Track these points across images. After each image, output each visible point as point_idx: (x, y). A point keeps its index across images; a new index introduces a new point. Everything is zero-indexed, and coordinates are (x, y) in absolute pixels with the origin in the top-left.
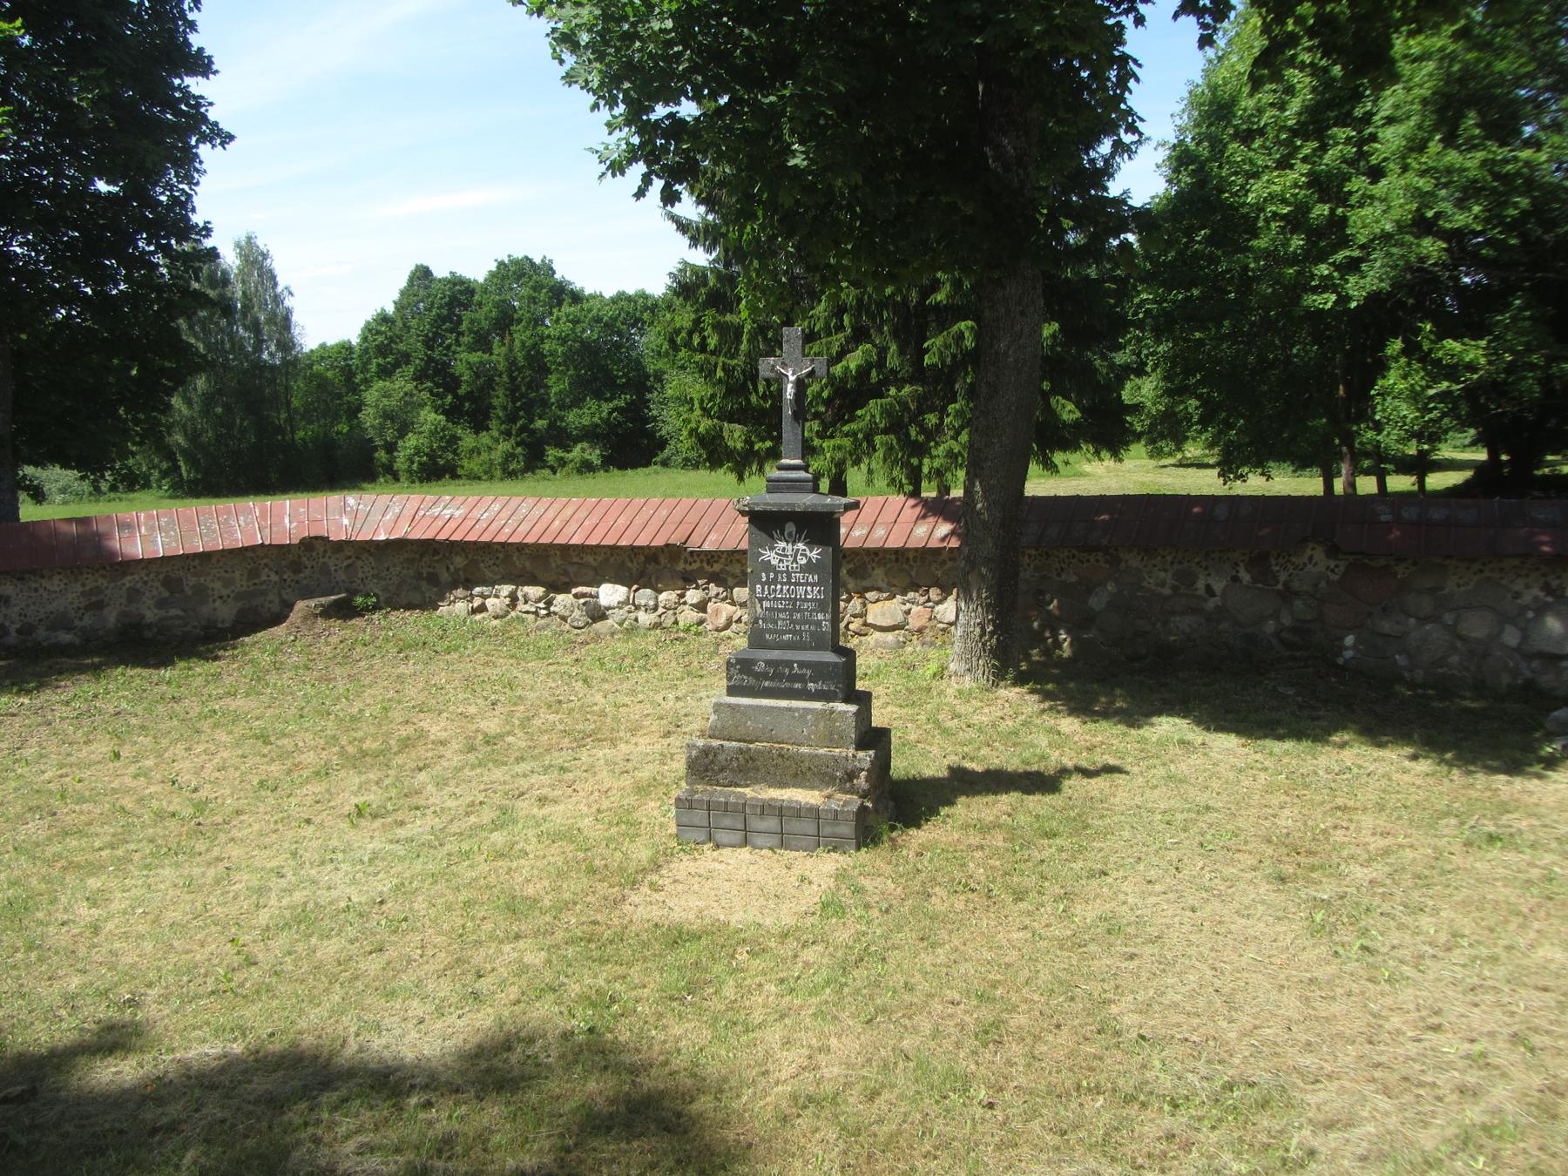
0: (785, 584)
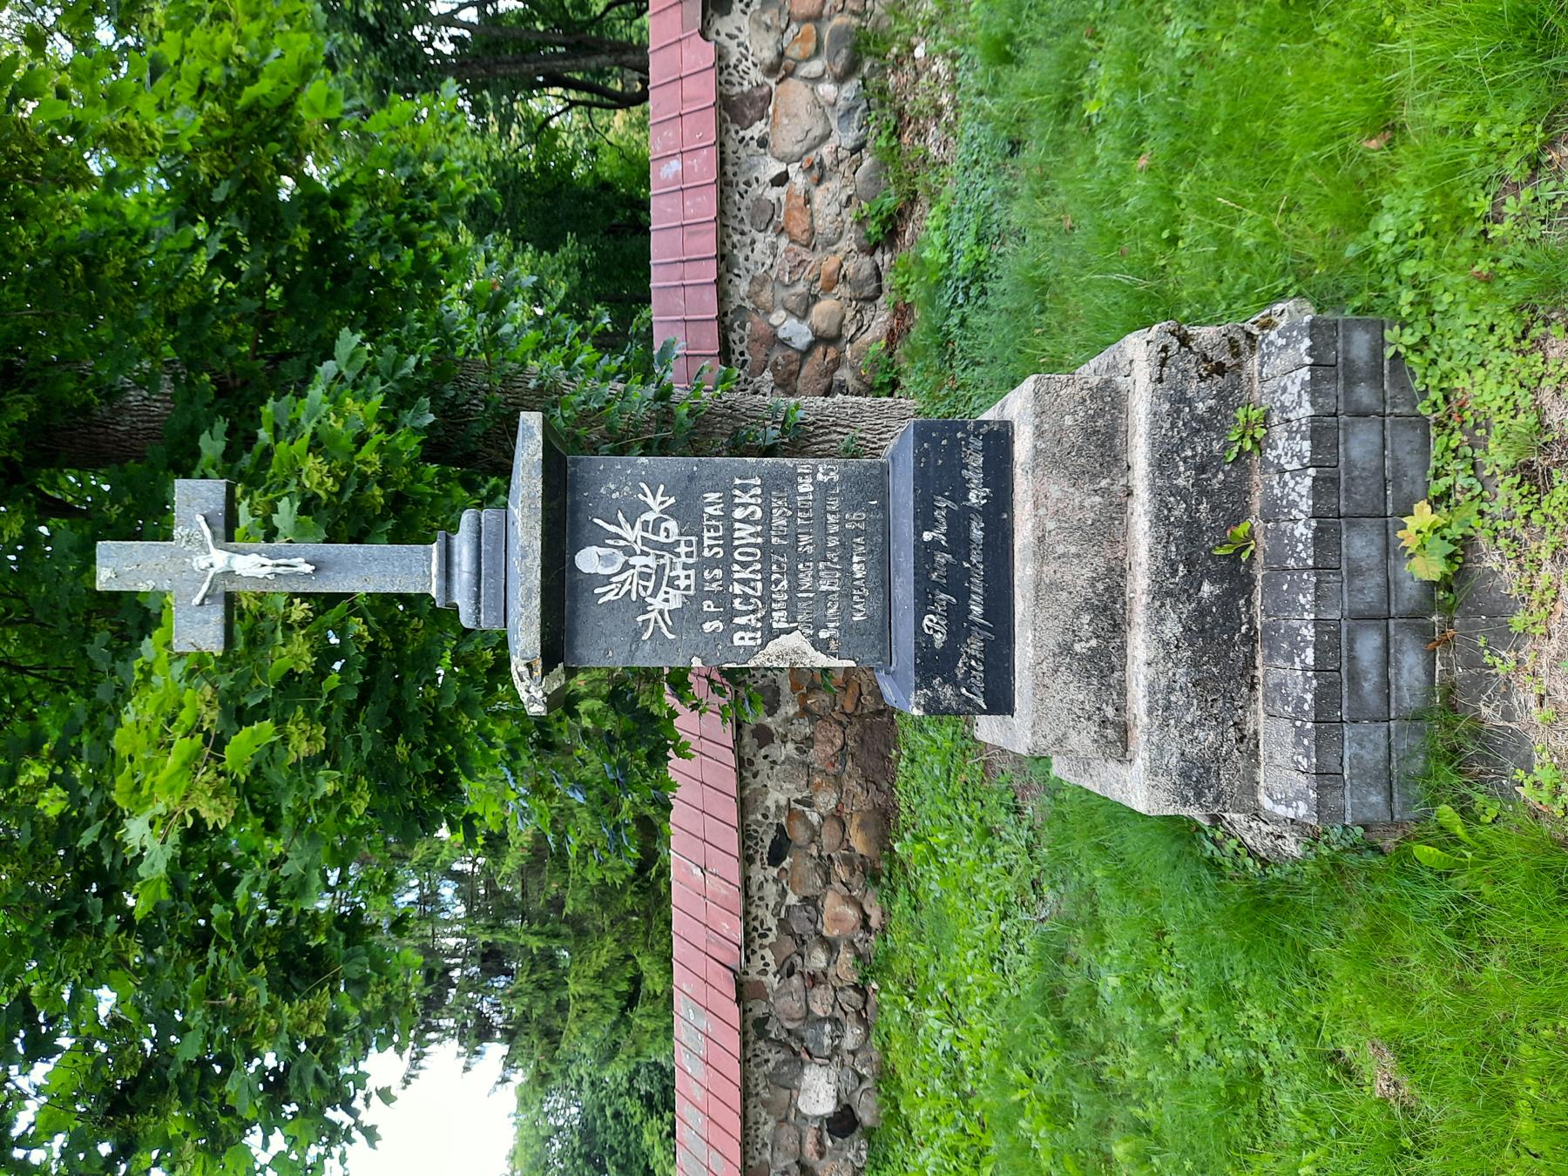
0: (728, 573)
